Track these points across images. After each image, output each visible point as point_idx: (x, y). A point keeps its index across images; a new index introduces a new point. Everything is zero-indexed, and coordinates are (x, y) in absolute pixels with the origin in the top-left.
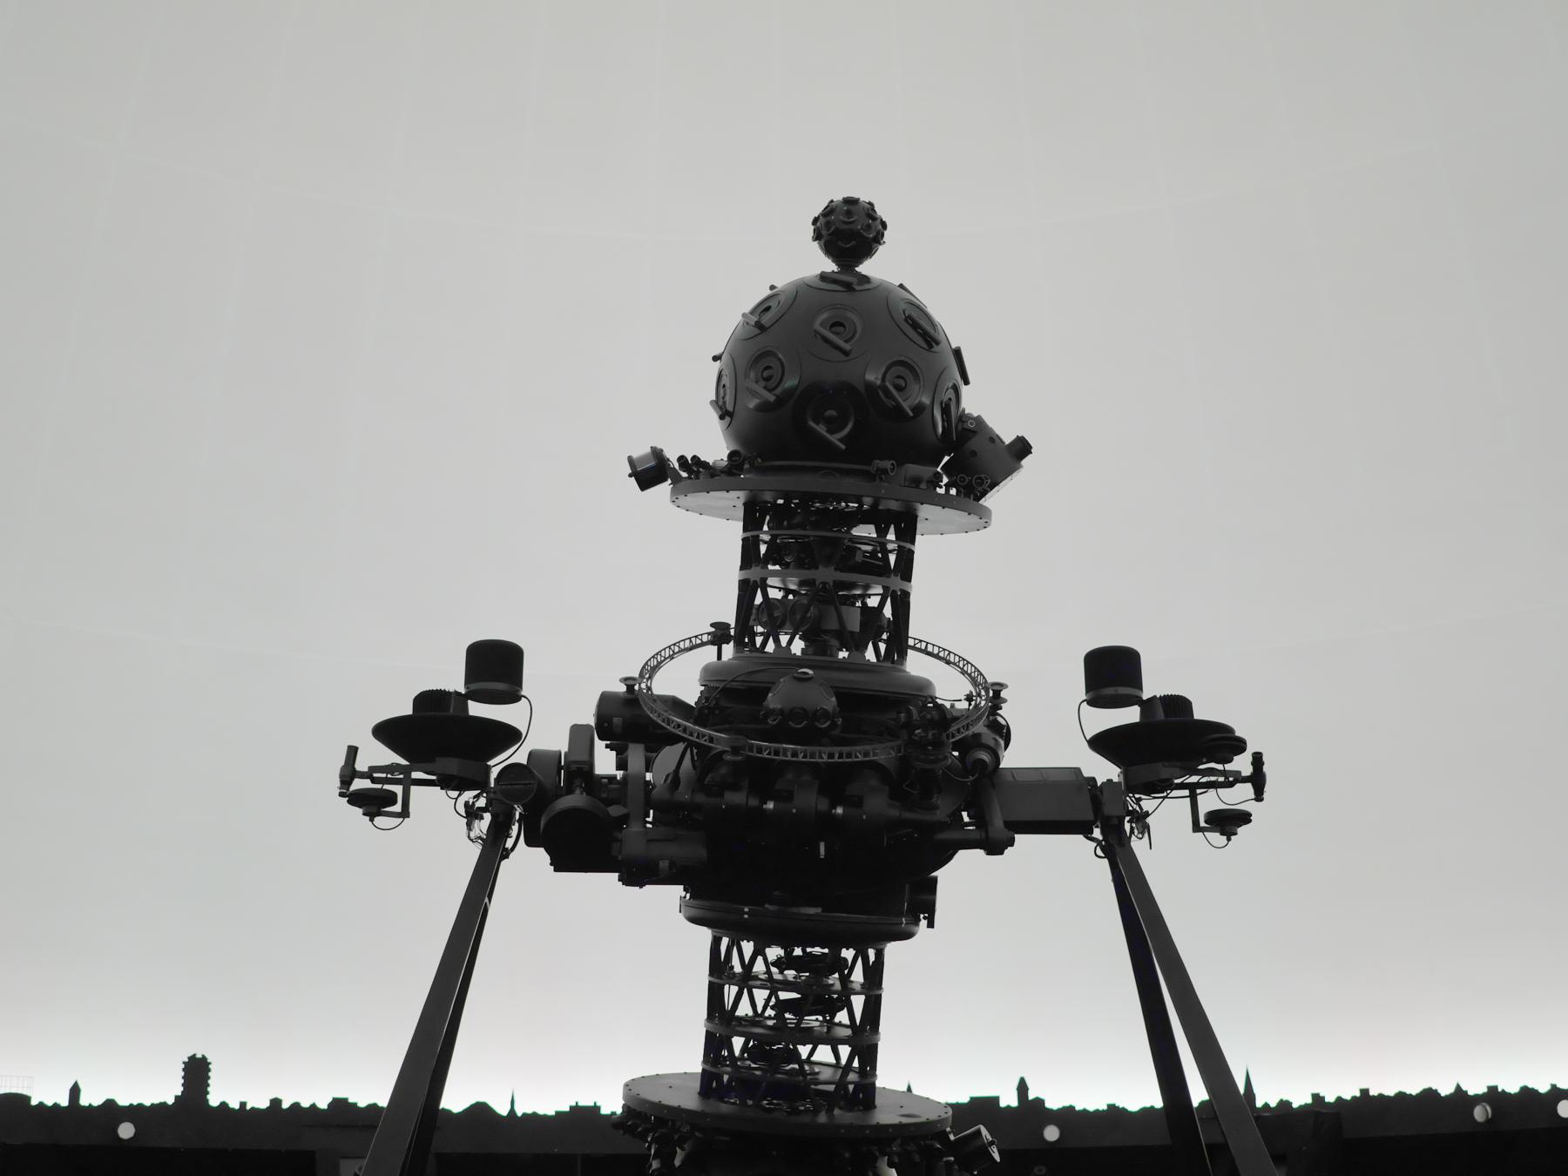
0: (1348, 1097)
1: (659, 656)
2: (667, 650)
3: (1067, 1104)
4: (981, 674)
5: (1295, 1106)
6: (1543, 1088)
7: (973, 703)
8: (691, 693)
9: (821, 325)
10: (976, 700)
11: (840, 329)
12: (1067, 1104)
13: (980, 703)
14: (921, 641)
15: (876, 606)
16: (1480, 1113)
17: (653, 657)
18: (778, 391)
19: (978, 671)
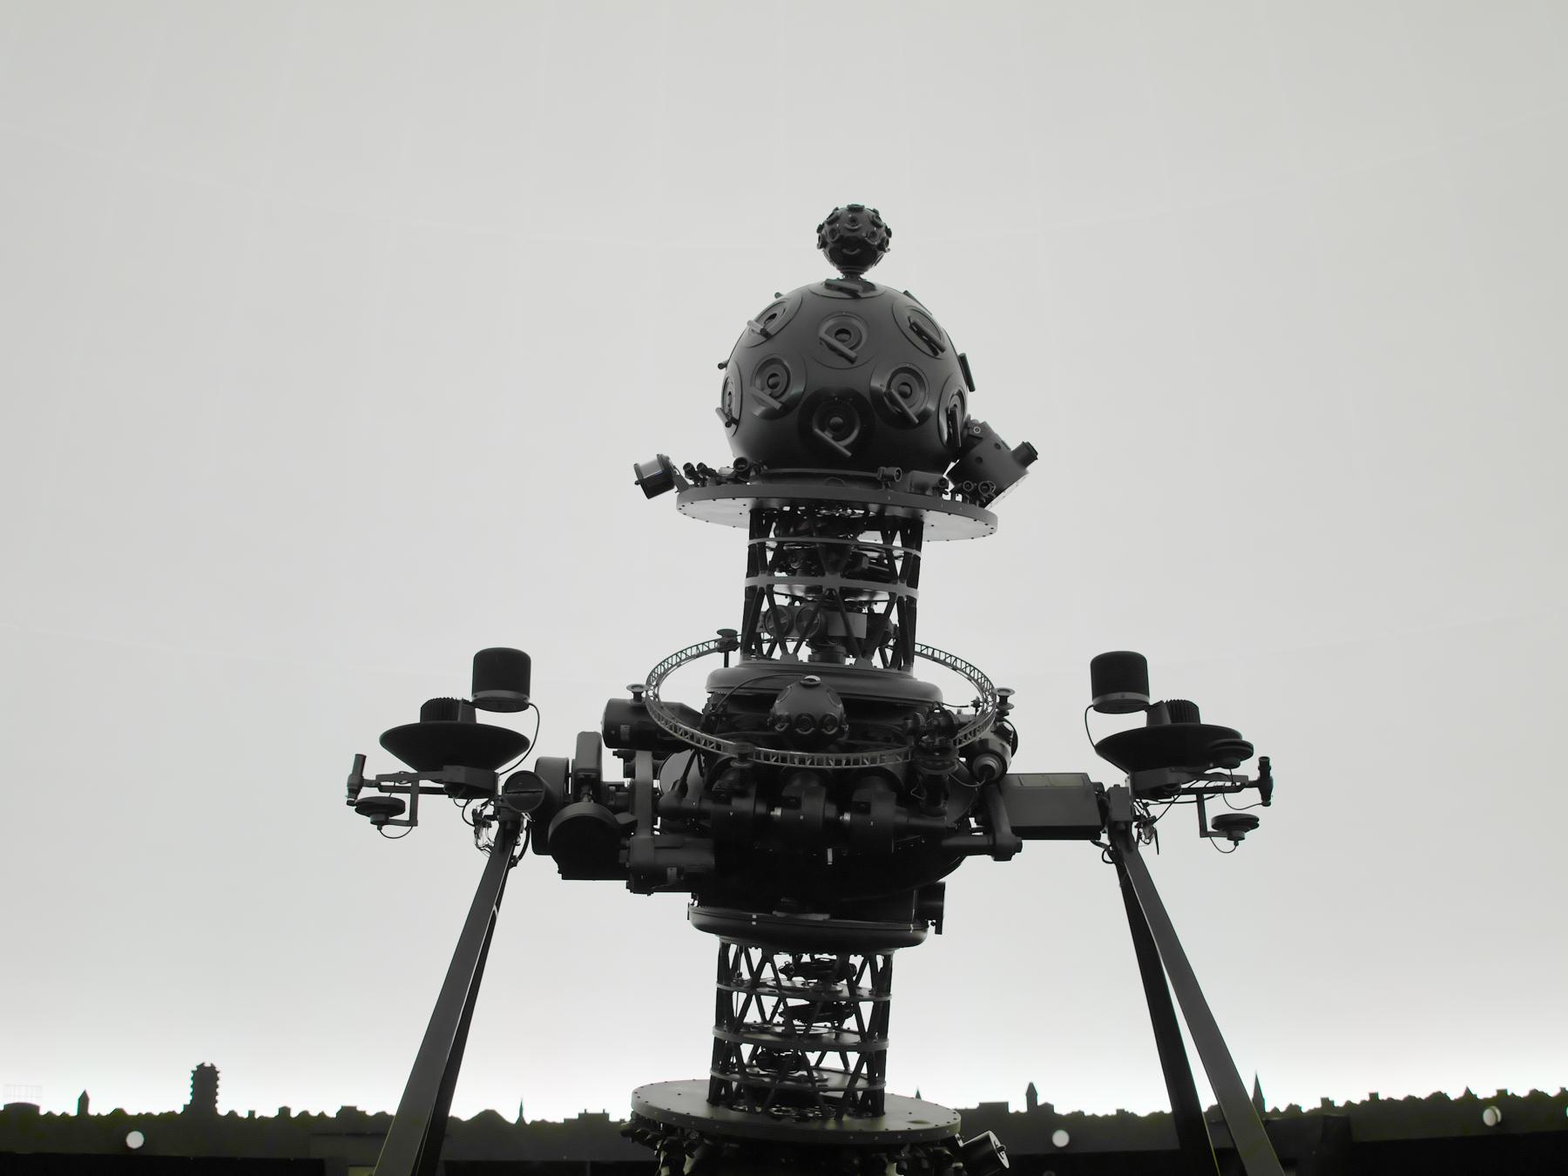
0: (1357, 1101)
1: (666, 664)
3: (1076, 1110)
4: (988, 680)
5: (1304, 1110)
7: (980, 709)
9: (826, 333)
11: (844, 336)
12: (1076, 1109)
13: (987, 709)
14: (927, 647)
15: (838, 1053)
18: (784, 399)
19: (985, 677)
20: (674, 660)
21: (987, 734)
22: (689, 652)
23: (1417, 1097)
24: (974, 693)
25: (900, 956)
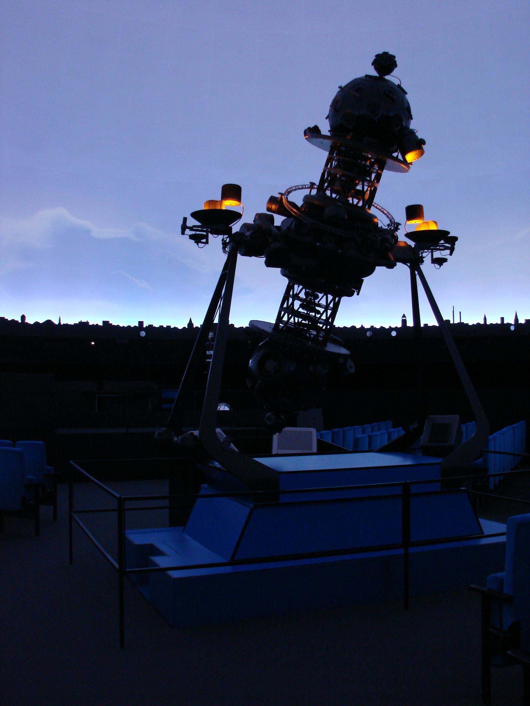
1: (291, 189)
2: (294, 187)
4: (393, 219)
6: (387, 327)
7: (389, 227)
8: (300, 203)
10: (390, 227)
13: (391, 228)
14: (376, 204)
16: (368, 334)
17: (290, 188)
19: (393, 217)
20: (294, 188)
21: (389, 236)
22: (299, 187)
23: (347, 327)
24: (388, 222)
25: (344, 299)
